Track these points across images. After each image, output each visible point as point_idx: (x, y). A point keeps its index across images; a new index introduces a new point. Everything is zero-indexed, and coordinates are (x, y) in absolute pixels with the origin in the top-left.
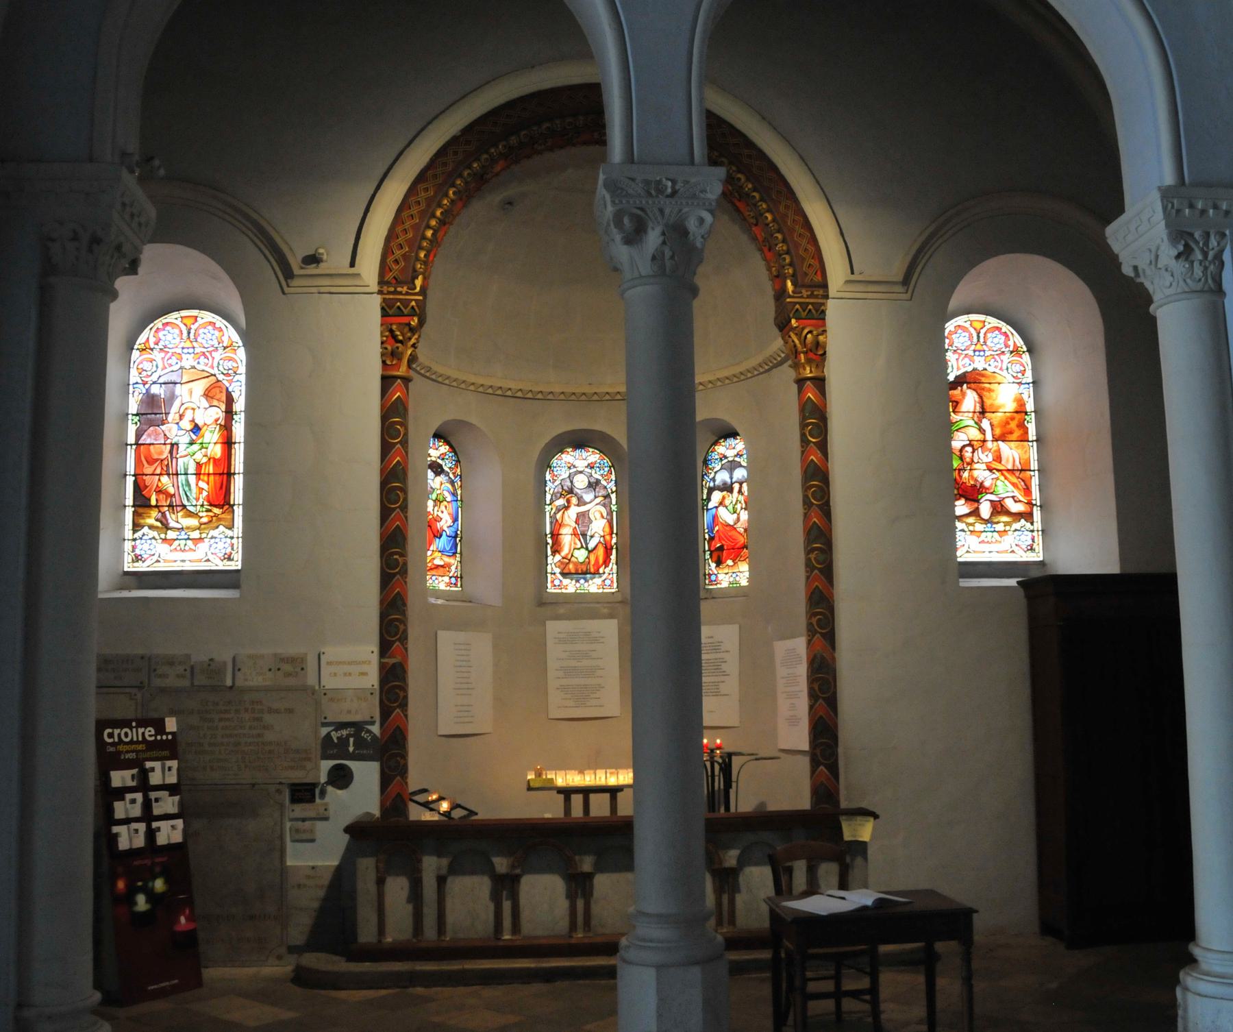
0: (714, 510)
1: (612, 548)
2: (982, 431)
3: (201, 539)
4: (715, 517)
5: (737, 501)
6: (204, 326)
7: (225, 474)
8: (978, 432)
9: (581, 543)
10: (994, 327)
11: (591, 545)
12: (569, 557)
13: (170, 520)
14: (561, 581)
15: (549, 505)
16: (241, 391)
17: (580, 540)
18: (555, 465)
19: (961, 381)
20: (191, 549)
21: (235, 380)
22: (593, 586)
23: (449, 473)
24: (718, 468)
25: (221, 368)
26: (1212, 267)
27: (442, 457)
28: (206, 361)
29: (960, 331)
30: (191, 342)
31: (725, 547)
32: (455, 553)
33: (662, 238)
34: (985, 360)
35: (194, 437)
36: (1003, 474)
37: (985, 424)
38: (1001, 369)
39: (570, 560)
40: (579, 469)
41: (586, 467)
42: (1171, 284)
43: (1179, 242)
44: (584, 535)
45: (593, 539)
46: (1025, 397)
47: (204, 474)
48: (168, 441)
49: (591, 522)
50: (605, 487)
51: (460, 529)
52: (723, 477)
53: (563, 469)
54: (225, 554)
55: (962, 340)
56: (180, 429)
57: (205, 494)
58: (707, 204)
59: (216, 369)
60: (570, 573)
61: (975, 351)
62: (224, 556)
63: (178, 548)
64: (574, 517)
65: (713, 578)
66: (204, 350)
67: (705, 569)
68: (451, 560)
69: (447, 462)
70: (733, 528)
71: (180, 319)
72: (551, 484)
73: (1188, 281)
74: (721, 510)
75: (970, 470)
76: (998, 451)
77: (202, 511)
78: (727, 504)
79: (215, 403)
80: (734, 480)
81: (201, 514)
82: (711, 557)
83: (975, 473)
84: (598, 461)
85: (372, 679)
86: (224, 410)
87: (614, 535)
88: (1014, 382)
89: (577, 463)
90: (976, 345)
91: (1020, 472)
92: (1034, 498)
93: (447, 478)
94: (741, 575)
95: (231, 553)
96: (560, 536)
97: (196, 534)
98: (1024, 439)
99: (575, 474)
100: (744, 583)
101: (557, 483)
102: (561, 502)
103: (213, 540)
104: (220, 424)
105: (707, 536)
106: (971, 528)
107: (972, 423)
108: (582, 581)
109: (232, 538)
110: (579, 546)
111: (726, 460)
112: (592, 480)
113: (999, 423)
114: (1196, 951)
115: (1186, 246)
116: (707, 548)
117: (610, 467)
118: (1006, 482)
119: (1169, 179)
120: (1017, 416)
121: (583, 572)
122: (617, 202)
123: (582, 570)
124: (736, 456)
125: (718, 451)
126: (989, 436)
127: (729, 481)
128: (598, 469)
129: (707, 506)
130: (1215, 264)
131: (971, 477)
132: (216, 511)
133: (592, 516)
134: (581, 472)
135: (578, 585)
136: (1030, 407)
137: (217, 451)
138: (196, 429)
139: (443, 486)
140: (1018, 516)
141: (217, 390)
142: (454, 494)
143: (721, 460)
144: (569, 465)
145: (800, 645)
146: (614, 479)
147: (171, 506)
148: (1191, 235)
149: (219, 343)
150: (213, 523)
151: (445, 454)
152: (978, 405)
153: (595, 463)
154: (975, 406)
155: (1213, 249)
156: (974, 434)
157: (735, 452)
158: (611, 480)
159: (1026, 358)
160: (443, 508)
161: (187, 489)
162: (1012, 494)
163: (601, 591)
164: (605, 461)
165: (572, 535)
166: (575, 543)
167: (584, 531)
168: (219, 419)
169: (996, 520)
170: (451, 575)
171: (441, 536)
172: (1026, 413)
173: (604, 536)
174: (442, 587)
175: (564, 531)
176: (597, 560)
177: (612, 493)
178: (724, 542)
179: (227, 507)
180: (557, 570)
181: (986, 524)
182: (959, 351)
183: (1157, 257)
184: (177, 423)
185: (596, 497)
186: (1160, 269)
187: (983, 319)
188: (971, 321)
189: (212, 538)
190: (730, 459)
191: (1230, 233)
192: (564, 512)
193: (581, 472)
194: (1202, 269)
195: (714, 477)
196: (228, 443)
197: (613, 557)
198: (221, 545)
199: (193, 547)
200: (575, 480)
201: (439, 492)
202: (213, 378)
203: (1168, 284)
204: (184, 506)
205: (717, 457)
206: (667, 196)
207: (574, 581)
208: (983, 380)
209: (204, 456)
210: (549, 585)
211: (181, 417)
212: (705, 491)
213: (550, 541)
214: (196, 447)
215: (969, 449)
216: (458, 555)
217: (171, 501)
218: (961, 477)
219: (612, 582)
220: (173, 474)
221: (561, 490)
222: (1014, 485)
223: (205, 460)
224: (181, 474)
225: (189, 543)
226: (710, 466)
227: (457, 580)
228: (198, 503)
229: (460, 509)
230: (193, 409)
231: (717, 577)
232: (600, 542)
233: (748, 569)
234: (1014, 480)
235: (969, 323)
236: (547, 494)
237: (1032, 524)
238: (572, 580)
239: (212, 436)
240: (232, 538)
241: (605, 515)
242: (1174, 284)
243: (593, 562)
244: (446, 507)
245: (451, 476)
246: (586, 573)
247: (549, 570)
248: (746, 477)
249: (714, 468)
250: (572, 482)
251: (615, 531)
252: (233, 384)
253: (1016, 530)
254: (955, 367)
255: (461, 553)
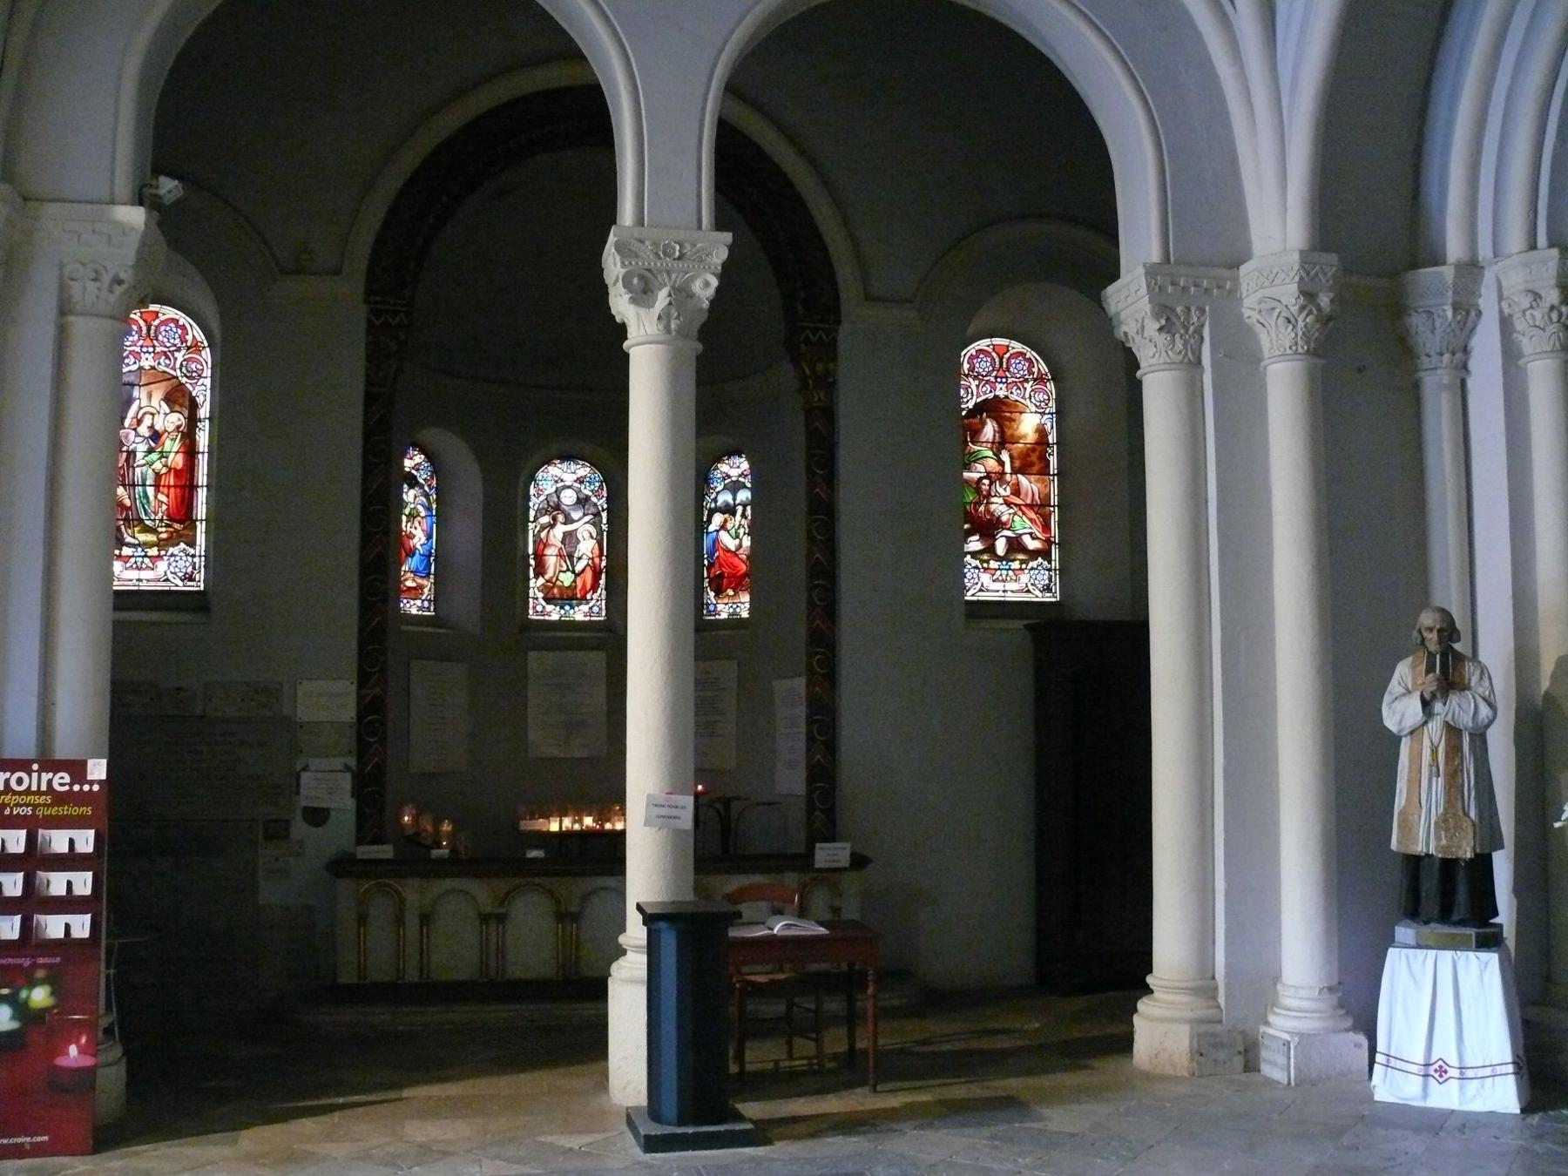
0: (715, 533)
1: (601, 572)
2: (1002, 463)
3: (159, 557)
4: (716, 541)
5: (740, 525)
6: (165, 322)
7: (185, 481)
8: (996, 464)
9: (567, 566)
10: (1018, 352)
11: (578, 568)
12: (554, 580)
13: (125, 535)
14: (544, 607)
15: (533, 522)
16: (205, 395)
17: (565, 562)
18: (540, 478)
19: (981, 408)
20: (148, 567)
21: (199, 383)
22: (579, 614)
23: (424, 485)
24: (720, 488)
25: (184, 370)
26: (1192, 341)
27: (417, 467)
28: (168, 362)
29: (981, 356)
30: (152, 340)
31: (726, 575)
32: (429, 574)
33: (668, 299)
34: (1007, 387)
35: (153, 444)
36: (1020, 509)
37: (1005, 457)
38: (1023, 397)
39: (554, 584)
40: (568, 484)
41: (575, 481)
42: (1154, 355)
43: (1162, 317)
44: (571, 556)
45: (580, 561)
46: (1048, 427)
47: (164, 486)
48: (125, 449)
49: (578, 542)
50: (595, 505)
51: (434, 547)
52: (726, 497)
53: (550, 483)
54: (186, 573)
55: (983, 364)
56: (137, 435)
57: (164, 507)
58: (713, 267)
59: (178, 371)
60: (555, 598)
61: (996, 377)
62: (184, 576)
63: (134, 566)
64: (560, 536)
65: (712, 608)
66: (167, 349)
67: (703, 599)
68: (425, 582)
69: (422, 473)
70: (735, 554)
71: (139, 314)
72: (536, 500)
73: (1170, 352)
74: (723, 534)
75: (987, 503)
76: (1018, 484)
77: (161, 527)
78: (729, 528)
79: (177, 408)
80: (737, 502)
81: (160, 530)
82: (710, 585)
83: (993, 507)
84: (589, 475)
85: (349, 714)
86: (186, 416)
87: (604, 558)
88: (1036, 412)
89: (565, 477)
90: (998, 371)
91: (1040, 507)
92: (1053, 535)
93: (422, 490)
94: (742, 606)
95: (193, 573)
96: (545, 557)
97: (154, 552)
98: (1044, 471)
99: (563, 490)
100: (745, 615)
101: (542, 498)
102: (545, 520)
103: (172, 559)
104: (182, 432)
105: (706, 562)
106: (985, 565)
107: (990, 453)
108: (567, 608)
109: (193, 556)
110: (565, 568)
111: (729, 480)
112: (581, 496)
113: (1019, 454)
114: (1149, 979)
115: (1168, 320)
116: (706, 575)
117: (602, 482)
118: (1024, 518)
119: (1155, 256)
120: (1039, 448)
121: (568, 597)
122: (627, 263)
123: (567, 595)
124: (740, 476)
125: (721, 469)
126: (1008, 468)
127: (732, 502)
128: (588, 484)
129: (707, 529)
130: (1194, 337)
131: (987, 510)
132: (177, 526)
133: (580, 537)
134: (569, 487)
135: (562, 612)
136: (1052, 438)
137: (178, 461)
138: (156, 436)
139: (417, 499)
140: (1034, 554)
141: (179, 394)
142: (429, 509)
143: (724, 479)
144: (556, 479)
145: (800, 684)
146: (605, 495)
147: (126, 520)
148: (1173, 310)
149: (182, 344)
150: (172, 540)
151: (419, 464)
152: (997, 435)
153: (585, 476)
154: (994, 436)
155: (1193, 324)
156: (992, 464)
157: (740, 471)
158: (603, 496)
159: (1051, 386)
160: (416, 524)
161: (144, 501)
162: (1030, 531)
163: (588, 619)
164: (596, 475)
165: (557, 556)
166: (561, 566)
167: (571, 552)
168: (181, 426)
169: (1012, 558)
170: (423, 598)
171: (414, 554)
172: (1048, 445)
173: (593, 559)
174: (414, 611)
175: (549, 551)
176: (584, 585)
177: (603, 510)
178: (724, 570)
179: (189, 522)
180: (540, 595)
181: (1001, 562)
182: (981, 377)
183: (1143, 327)
184: (135, 430)
185: (585, 515)
186: (1145, 338)
187: (1007, 344)
188: (994, 345)
189: (172, 555)
190: (734, 479)
191: (1210, 309)
192: (549, 531)
193: (569, 487)
194: (1182, 342)
195: (716, 497)
196: (190, 451)
197: (602, 582)
198: (181, 564)
199: (151, 565)
200: (562, 495)
201: (412, 506)
202: (175, 380)
203: (1151, 354)
204: (141, 521)
205: (719, 476)
206: (674, 259)
207: (558, 608)
208: (1004, 408)
209: (164, 466)
210: (531, 612)
211: (139, 422)
212: (706, 513)
213: (532, 562)
214: (154, 456)
215: (986, 482)
216: (432, 576)
217: (127, 515)
218: (976, 511)
219: (600, 609)
220: (129, 485)
221: (546, 506)
222: (1031, 520)
223: (164, 470)
224: (138, 485)
225: (147, 560)
226: (712, 486)
227: (430, 604)
228: (157, 518)
229: (435, 525)
230: (153, 414)
231: (716, 607)
232: (588, 565)
233: (748, 600)
234: (1033, 516)
235: (992, 347)
236: (531, 510)
237: (1050, 563)
238: (556, 606)
239: (172, 445)
240: (193, 556)
241: (594, 535)
242: (1157, 355)
243: (579, 587)
244: (420, 523)
245: (426, 488)
246: (572, 599)
247: (531, 595)
248: (750, 498)
249: (716, 487)
250: (558, 497)
251: (605, 554)
252: (198, 388)
253: (1032, 569)
254: (975, 393)
255: (435, 574)
